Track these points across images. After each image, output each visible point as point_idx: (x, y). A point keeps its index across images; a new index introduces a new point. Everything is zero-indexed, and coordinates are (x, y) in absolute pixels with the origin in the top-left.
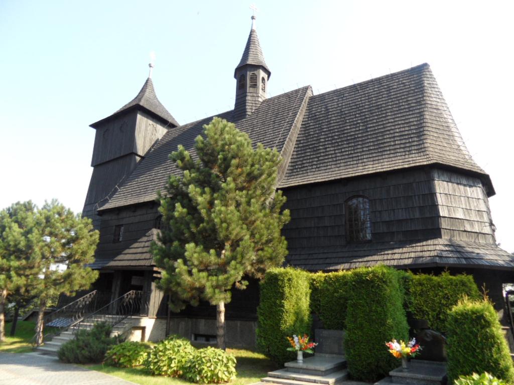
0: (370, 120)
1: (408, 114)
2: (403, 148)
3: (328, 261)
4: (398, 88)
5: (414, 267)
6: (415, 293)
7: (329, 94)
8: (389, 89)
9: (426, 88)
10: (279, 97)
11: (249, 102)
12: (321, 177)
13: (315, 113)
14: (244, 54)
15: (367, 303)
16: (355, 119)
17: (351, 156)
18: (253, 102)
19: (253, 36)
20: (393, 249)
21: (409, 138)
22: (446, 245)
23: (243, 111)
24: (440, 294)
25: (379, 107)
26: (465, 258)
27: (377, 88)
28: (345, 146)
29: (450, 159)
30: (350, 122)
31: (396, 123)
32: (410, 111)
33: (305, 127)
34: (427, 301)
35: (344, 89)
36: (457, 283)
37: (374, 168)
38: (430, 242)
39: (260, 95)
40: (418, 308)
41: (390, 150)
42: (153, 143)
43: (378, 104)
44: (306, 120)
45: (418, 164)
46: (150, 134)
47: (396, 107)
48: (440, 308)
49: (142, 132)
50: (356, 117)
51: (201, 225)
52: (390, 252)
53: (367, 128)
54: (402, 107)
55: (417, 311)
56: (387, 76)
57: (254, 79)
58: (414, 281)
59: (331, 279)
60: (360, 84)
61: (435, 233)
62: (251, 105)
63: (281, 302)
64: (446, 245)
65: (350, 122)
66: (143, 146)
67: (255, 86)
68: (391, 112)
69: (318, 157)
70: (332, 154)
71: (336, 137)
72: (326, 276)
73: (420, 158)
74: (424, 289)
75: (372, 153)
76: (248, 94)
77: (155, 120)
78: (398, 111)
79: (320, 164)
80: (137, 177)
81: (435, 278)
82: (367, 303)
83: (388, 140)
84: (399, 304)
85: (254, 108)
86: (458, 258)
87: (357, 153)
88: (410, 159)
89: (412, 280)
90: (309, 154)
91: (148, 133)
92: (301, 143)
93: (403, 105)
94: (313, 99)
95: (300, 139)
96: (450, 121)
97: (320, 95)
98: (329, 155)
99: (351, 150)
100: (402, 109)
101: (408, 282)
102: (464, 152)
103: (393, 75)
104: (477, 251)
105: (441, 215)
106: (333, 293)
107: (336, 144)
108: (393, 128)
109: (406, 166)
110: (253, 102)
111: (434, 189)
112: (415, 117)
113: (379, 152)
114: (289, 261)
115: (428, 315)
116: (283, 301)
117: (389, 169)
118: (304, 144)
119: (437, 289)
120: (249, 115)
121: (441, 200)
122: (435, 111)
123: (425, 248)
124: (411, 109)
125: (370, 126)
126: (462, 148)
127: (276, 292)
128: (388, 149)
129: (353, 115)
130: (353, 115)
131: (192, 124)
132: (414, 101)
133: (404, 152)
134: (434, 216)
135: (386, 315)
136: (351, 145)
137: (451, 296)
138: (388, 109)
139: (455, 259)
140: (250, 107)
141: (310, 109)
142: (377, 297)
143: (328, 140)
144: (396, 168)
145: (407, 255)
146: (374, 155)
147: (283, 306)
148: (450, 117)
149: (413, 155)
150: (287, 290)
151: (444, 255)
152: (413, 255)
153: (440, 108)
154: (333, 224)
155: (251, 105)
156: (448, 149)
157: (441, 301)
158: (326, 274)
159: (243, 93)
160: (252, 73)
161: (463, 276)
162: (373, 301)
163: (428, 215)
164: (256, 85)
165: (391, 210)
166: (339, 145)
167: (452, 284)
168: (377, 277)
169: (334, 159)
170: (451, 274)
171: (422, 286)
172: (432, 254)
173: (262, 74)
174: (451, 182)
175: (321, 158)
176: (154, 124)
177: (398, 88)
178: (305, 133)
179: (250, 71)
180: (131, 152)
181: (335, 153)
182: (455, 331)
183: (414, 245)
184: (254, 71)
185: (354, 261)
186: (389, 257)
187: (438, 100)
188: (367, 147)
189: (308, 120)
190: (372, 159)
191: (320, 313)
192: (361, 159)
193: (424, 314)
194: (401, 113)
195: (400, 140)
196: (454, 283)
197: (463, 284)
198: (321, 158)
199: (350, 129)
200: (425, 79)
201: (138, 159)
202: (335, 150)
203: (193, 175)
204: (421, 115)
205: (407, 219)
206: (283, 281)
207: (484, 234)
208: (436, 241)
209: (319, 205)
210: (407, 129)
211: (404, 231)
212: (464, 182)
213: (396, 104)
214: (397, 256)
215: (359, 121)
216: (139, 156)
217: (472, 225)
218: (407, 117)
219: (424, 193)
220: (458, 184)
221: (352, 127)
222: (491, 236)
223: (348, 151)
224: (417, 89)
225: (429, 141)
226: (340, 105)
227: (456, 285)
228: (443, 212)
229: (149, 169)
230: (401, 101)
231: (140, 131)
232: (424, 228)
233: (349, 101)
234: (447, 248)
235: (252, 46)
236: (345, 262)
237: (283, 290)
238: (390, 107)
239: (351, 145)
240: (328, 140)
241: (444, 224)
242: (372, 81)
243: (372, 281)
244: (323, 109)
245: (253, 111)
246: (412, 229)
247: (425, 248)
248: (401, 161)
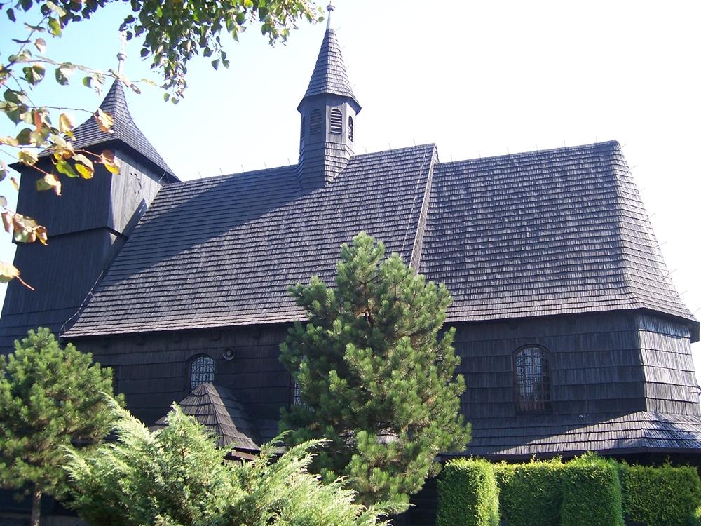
0: (541, 224)
1: (597, 222)
2: (595, 278)
3: (493, 442)
4: (578, 175)
5: (617, 453)
6: (632, 490)
7: (468, 163)
8: (565, 174)
9: (619, 183)
10: (381, 156)
11: (330, 159)
12: (477, 313)
13: (449, 196)
14: (315, 72)
15: (590, 507)
16: (517, 219)
17: (518, 281)
18: (336, 160)
19: (331, 41)
20: (585, 425)
21: (601, 263)
22: (653, 422)
23: (319, 174)
24: (662, 490)
25: (552, 203)
26: (676, 440)
27: (546, 168)
28: (506, 262)
29: (656, 302)
30: (509, 222)
31: (582, 235)
32: (599, 218)
33: (435, 219)
34: (647, 500)
35: (492, 160)
36: (681, 477)
37: (558, 307)
38: (633, 416)
39: (346, 149)
40: (636, 509)
41: (576, 279)
42: (137, 207)
43: (551, 197)
44: (435, 206)
45: (619, 308)
46: (131, 193)
47: (579, 208)
48: (661, 507)
49: (120, 189)
50: (518, 215)
51: (368, 403)
52: (582, 430)
53: (538, 237)
54: (588, 210)
55: (634, 512)
56: (559, 151)
57: (338, 118)
58: (631, 475)
59: (525, 473)
60: (519, 157)
61: (639, 404)
62: (333, 164)
63: (473, 508)
64: (653, 422)
65: (509, 222)
66: (122, 214)
67: (338, 131)
68: (572, 215)
69: (465, 277)
70: (487, 274)
71: (490, 246)
72: (517, 469)
73: (620, 297)
74: (644, 485)
75: (550, 281)
76: (328, 145)
77: (138, 166)
78: (581, 214)
79: (471, 288)
80: (125, 275)
81: (656, 471)
82: (590, 507)
83: (573, 262)
84: (620, 503)
85: (337, 170)
86: (670, 439)
87: (527, 277)
88: (608, 298)
89: (629, 475)
90: (448, 268)
91: (130, 191)
92: (431, 248)
93: (588, 207)
94: (440, 167)
95: (429, 240)
96: (651, 238)
97: (452, 163)
98: (482, 274)
99: (517, 271)
100: (588, 213)
101: (624, 476)
102: (671, 287)
103: (568, 151)
104: (687, 429)
105: (647, 380)
106: (530, 492)
107: (493, 258)
108: (577, 242)
109: (603, 309)
110: (336, 160)
111: (639, 344)
112: (607, 230)
113: (560, 280)
114: (473, 451)
115: (648, 516)
116: (476, 506)
117: (579, 311)
118: (438, 251)
119: (658, 484)
120: (330, 183)
121: (646, 358)
122: (633, 222)
123: (628, 426)
124: (601, 215)
125: (542, 233)
126: (667, 281)
127: (464, 494)
128: (573, 276)
129: (513, 210)
130: (513, 210)
131: (213, 180)
132: (604, 203)
133: (598, 284)
134: (638, 381)
135: (613, 521)
136: (516, 262)
137: (675, 493)
138: (567, 209)
139: (666, 441)
140: (332, 169)
141: (438, 188)
142: (601, 499)
143: (479, 249)
144: (589, 310)
145: (605, 436)
146: (554, 284)
147: (476, 513)
148: (650, 232)
149: (611, 292)
150: (479, 490)
151: (653, 437)
152: (614, 436)
153: (639, 217)
154: (496, 386)
155: (333, 164)
156: (652, 283)
157: (663, 499)
158: (515, 466)
159: (318, 143)
160: (333, 108)
161: (685, 468)
162: (598, 504)
163: (630, 379)
164: (341, 130)
165: (579, 369)
166: (496, 260)
167: (675, 478)
168: (602, 474)
169: (493, 283)
170: (674, 465)
171: (641, 481)
172: (639, 434)
173: (350, 111)
174: (658, 333)
175: (470, 279)
176: (138, 172)
177: (578, 175)
178: (437, 231)
179: (331, 105)
180: (105, 225)
181: (492, 273)
182: (61, 415)
183: (613, 421)
184: (337, 105)
185: (534, 442)
186: (583, 437)
187: (636, 204)
188: (542, 269)
189: (439, 208)
190: (551, 291)
191: (509, 518)
192: (536, 289)
193: (643, 516)
194: (586, 219)
195: (590, 264)
196: (678, 478)
197: (688, 478)
198: (470, 279)
199: (512, 234)
200: (617, 168)
201: (113, 237)
202: (491, 268)
203: (347, 328)
204: (616, 227)
205: (601, 384)
206: (474, 479)
207: (692, 403)
208: (640, 415)
209: (473, 355)
210: (598, 247)
211: (598, 400)
212: (672, 332)
213: (578, 203)
214: (592, 437)
215: (525, 223)
216: (116, 233)
217: (679, 392)
218: (597, 228)
219: (625, 348)
220: (664, 334)
221: (514, 231)
222: (290, 155)
223: (513, 272)
224: (606, 182)
225: (629, 271)
226: (490, 189)
227: (680, 481)
228: (649, 376)
229: (148, 261)
230: (585, 199)
231: (117, 188)
232: (624, 397)
233: (503, 184)
234: (654, 426)
235: (331, 60)
236: (520, 443)
237: (475, 492)
238: (570, 206)
239: (516, 262)
240: (479, 249)
241: (650, 393)
242: (536, 155)
243: (597, 480)
244: (462, 192)
245: (337, 175)
246: (609, 398)
247: (628, 426)
248: (594, 299)
